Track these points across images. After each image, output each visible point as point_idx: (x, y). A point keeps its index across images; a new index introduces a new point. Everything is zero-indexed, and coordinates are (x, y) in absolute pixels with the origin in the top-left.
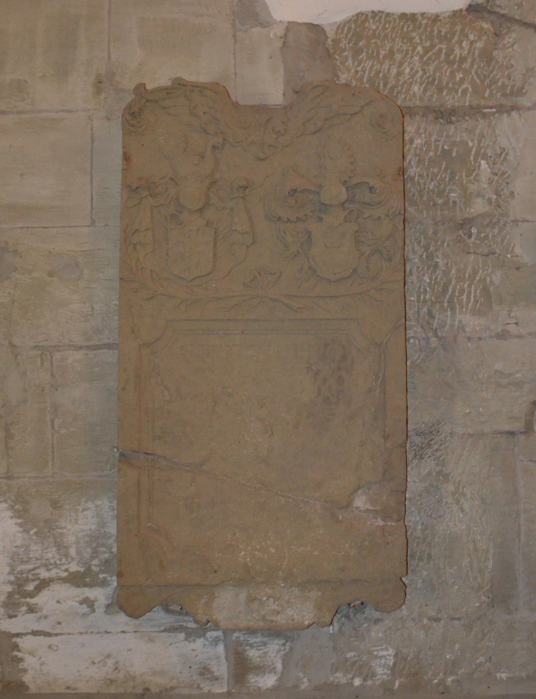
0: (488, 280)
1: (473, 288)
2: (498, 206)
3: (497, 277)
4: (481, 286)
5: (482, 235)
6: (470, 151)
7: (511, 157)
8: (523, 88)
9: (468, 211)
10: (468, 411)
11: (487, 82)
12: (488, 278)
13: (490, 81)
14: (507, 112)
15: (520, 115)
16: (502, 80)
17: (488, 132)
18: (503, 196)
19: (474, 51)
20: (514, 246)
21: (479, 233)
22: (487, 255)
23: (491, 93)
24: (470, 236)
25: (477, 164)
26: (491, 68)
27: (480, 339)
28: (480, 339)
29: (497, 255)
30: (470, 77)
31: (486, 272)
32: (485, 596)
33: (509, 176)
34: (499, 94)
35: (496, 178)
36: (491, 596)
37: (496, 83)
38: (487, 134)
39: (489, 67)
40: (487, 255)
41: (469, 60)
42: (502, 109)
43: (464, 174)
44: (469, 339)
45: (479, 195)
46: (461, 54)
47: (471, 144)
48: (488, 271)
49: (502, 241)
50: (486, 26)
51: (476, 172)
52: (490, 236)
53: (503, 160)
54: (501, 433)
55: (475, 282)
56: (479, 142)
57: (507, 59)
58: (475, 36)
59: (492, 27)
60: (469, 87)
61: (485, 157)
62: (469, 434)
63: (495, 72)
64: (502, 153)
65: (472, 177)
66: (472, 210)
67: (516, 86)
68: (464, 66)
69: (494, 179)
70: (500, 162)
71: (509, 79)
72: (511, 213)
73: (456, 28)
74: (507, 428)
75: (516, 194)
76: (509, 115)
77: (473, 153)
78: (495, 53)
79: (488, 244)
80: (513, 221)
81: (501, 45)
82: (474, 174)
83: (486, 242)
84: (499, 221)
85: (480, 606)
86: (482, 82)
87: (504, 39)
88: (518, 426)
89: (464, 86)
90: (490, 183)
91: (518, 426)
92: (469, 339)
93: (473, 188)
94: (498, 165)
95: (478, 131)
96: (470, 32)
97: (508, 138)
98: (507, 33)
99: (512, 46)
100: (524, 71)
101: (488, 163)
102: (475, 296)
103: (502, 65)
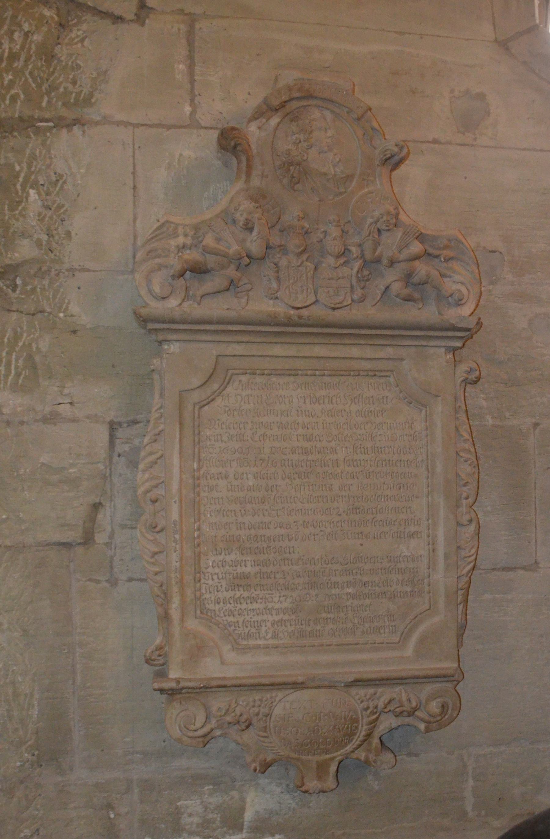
0: (34, 346)
1: (14, 357)
2: (50, 250)
3: (44, 344)
4: (25, 354)
5: (29, 288)
6: (17, 177)
7: (69, 186)
8: (91, 95)
9: (9, 256)
10: (4, 517)
11: (45, 86)
12: (33, 344)
13: (49, 86)
14: (67, 126)
15: (84, 132)
16: (64, 84)
17: (41, 152)
18: (57, 237)
19: (30, 45)
20: (69, 303)
21: (25, 284)
22: (33, 315)
23: (49, 102)
24: (14, 290)
25: (25, 195)
26: (51, 69)
27: (22, 423)
28: (22, 423)
29: (46, 314)
30: (23, 79)
31: (32, 336)
32: (28, 753)
33: (66, 210)
34: (60, 103)
35: (49, 213)
36: (36, 753)
37: (57, 88)
38: (40, 156)
39: (48, 68)
40: (33, 315)
41: (23, 58)
42: (62, 123)
43: (6, 207)
44: (8, 423)
45: (24, 235)
46: (10, 49)
47: (17, 168)
48: (34, 334)
49: (54, 297)
50: (47, 13)
51: (23, 204)
52: (38, 290)
53: (60, 190)
54: (49, 545)
55: (17, 349)
56: (30, 166)
57: (74, 58)
58: (30, 25)
59: (58, 15)
60: (21, 92)
61: (35, 185)
62: (6, 547)
63: (56, 74)
64: (58, 181)
65: (17, 212)
66: (16, 255)
67: (83, 93)
68: (15, 65)
69: (46, 215)
70: (55, 192)
71: (74, 83)
72: (66, 260)
73: (6, 14)
74: (57, 537)
75: (73, 234)
76: (69, 131)
77: (21, 179)
78: (57, 49)
79: (35, 299)
80: (69, 270)
81: (66, 41)
82: (20, 208)
83: (33, 297)
84: (49, 271)
85: (21, 766)
86: (39, 86)
87: (71, 31)
88: (73, 535)
89: (13, 92)
90: (41, 220)
91: (73, 535)
92: (8, 423)
93: (17, 225)
94: (53, 195)
95: (28, 151)
96: (24, 20)
97: (66, 161)
98: (75, 25)
99: (82, 41)
100: (95, 75)
101: (39, 194)
102: (17, 367)
103: (67, 65)
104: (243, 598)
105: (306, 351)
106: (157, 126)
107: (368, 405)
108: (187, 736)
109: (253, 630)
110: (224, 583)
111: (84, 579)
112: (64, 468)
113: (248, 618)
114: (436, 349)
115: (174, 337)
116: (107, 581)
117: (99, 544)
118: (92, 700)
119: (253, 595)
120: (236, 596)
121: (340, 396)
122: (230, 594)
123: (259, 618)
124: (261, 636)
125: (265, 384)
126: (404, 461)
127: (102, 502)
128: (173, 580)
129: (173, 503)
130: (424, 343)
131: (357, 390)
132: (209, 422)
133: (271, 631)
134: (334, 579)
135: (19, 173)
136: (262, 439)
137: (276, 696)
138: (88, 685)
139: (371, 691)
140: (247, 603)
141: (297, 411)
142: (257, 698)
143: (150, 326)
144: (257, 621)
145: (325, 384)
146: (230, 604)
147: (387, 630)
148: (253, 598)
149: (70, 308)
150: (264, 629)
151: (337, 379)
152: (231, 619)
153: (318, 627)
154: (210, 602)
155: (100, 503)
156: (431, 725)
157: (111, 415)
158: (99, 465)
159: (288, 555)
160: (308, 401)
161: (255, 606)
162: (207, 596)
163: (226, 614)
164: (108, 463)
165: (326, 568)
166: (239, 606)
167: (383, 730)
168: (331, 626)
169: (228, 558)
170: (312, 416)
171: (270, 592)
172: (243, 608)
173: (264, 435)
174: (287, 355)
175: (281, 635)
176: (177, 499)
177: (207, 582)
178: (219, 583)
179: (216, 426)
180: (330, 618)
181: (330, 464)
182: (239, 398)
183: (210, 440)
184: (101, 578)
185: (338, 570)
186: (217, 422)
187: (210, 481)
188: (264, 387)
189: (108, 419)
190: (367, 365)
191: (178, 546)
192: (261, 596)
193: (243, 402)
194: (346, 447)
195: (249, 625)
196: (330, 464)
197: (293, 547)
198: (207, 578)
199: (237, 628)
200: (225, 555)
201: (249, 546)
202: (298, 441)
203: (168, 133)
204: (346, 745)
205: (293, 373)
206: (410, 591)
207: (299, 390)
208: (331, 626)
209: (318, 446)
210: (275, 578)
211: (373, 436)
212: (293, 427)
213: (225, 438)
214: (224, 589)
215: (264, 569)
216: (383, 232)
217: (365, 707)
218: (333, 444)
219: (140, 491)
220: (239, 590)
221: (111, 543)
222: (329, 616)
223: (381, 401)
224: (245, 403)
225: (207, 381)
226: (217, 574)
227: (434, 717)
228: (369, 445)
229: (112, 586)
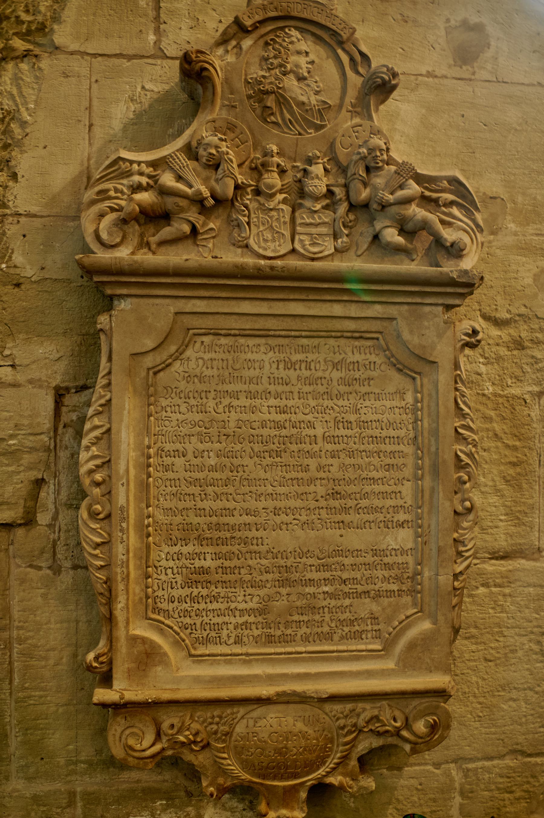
20: (12, 253)
104: (202, 596)
105: (279, 308)
106: (116, 56)
107: (352, 372)
108: (134, 757)
109: (213, 634)
110: (179, 578)
111: (24, 565)
113: (206, 620)
114: (433, 307)
115: (124, 291)
116: (49, 568)
117: (42, 525)
118: (32, 702)
119: (213, 593)
120: (193, 595)
121: (319, 361)
122: (187, 591)
123: (220, 620)
124: (222, 641)
125: (231, 346)
126: (393, 437)
127: (45, 477)
128: (119, 575)
129: (120, 486)
130: (419, 300)
131: (340, 354)
132: (165, 391)
133: (233, 635)
134: (309, 576)
136: (227, 409)
137: (238, 712)
138: (27, 685)
139: (349, 706)
140: (206, 603)
141: (269, 377)
142: (215, 713)
143: (96, 279)
144: (218, 624)
145: (302, 346)
146: (186, 603)
147: (369, 635)
148: (214, 596)
149: (13, 258)
150: (225, 633)
151: (316, 341)
152: (188, 620)
153: (289, 632)
154: (162, 600)
155: (43, 479)
156: (417, 746)
157: (57, 381)
158: (43, 436)
159: (255, 548)
160: (281, 366)
161: (215, 606)
162: (160, 593)
163: (182, 615)
164: (52, 434)
165: (300, 563)
166: (196, 606)
167: (362, 750)
168: (304, 630)
169: (185, 550)
170: (287, 385)
171: (233, 590)
172: (201, 609)
173: (230, 406)
174: (257, 312)
175: (245, 639)
176: (124, 481)
177: (159, 577)
178: (174, 579)
179: (173, 395)
180: (303, 621)
181: (307, 440)
182: (201, 362)
183: (166, 412)
184: (43, 565)
185: (313, 565)
186: (174, 390)
187: (165, 459)
188: (230, 349)
189: (54, 384)
190: (351, 325)
191: (125, 536)
192: (222, 595)
193: (205, 366)
194: (326, 421)
195: (207, 627)
196: (307, 440)
197: (261, 538)
198: (159, 572)
199: (194, 631)
200: (182, 546)
201: (209, 536)
202: (269, 413)
203: (129, 64)
204: (318, 768)
205: (264, 334)
206: (398, 590)
207: (271, 354)
208: (304, 630)
209: (293, 420)
210: (240, 574)
211: (358, 407)
212: (264, 397)
213: (183, 409)
214: (179, 586)
215: (227, 563)
216: (372, 170)
217: (342, 725)
218: (310, 417)
219: (83, 470)
220: (197, 588)
221: (55, 525)
222: (301, 618)
223: (368, 367)
224: (207, 368)
225: (162, 343)
226: (172, 568)
227: (421, 738)
228: (352, 418)
229: (54, 574)
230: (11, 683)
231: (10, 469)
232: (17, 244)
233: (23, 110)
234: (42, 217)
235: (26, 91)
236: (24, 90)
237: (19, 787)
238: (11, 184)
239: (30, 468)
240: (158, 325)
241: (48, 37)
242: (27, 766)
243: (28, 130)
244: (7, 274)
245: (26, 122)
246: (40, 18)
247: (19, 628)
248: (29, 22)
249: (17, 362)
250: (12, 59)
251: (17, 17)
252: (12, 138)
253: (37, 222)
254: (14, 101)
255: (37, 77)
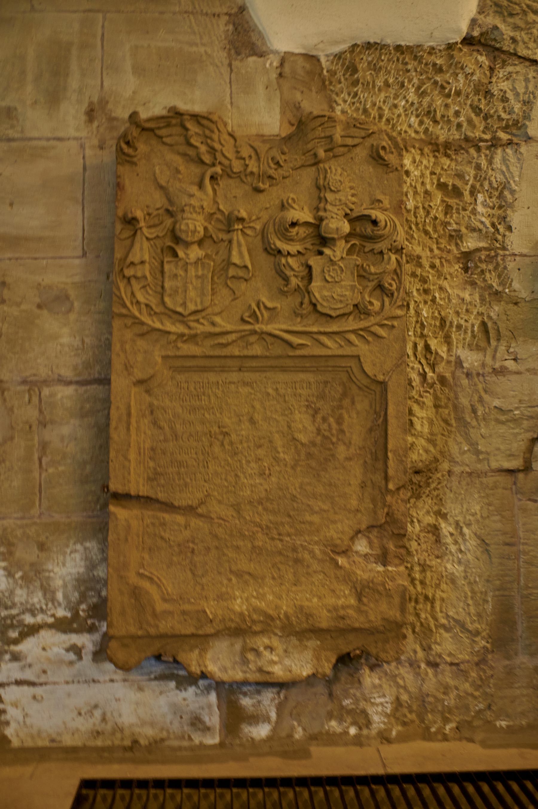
20: (512, 281)
112: (511, 411)
135: (468, 181)
230: (518, 584)
231: (515, 431)
232: (515, 275)
233: (511, 182)
234: (530, 256)
235: (513, 169)
236: (511, 168)
237: (525, 661)
238: (507, 233)
239: (527, 431)
240: (496, 308)
241: (522, 130)
242: (530, 645)
243: (516, 196)
244: (509, 296)
245: (515, 191)
246: (514, 116)
247: (524, 544)
248: (508, 120)
249: (519, 357)
250: (500, 146)
251: (499, 116)
252: (506, 202)
253: (527, 260)
254: (505, 176)
255: (519, 159)
